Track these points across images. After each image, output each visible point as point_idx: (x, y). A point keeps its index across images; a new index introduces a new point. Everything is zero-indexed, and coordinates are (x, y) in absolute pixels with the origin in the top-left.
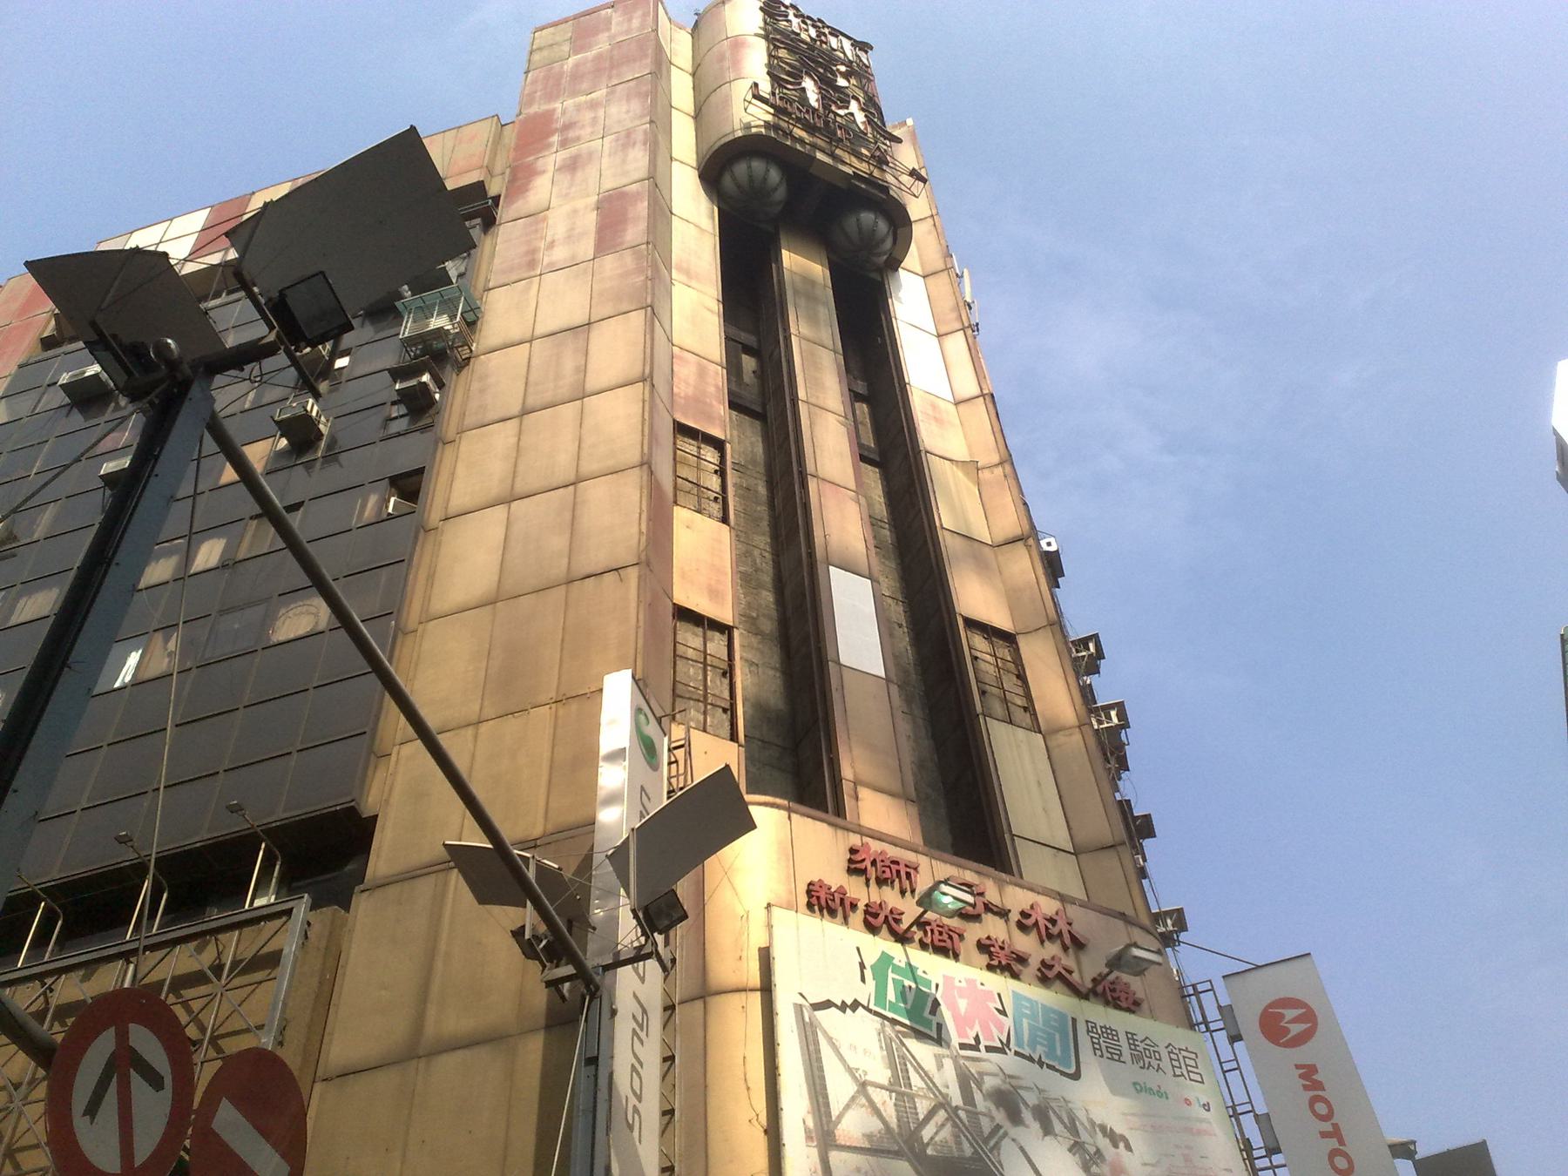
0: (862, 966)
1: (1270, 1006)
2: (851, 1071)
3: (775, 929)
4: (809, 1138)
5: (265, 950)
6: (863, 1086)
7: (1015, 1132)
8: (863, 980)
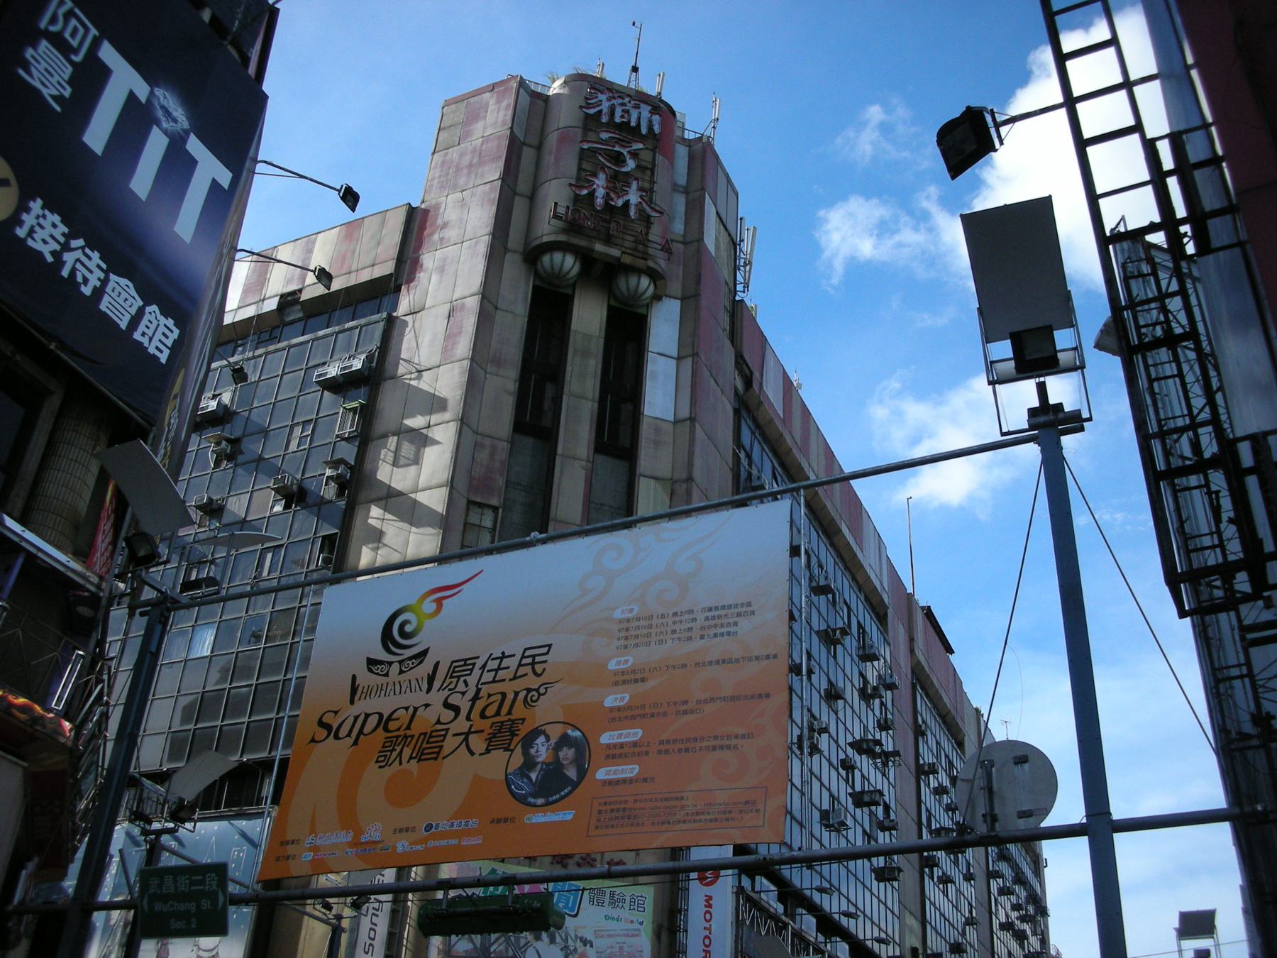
7: (538, 945)
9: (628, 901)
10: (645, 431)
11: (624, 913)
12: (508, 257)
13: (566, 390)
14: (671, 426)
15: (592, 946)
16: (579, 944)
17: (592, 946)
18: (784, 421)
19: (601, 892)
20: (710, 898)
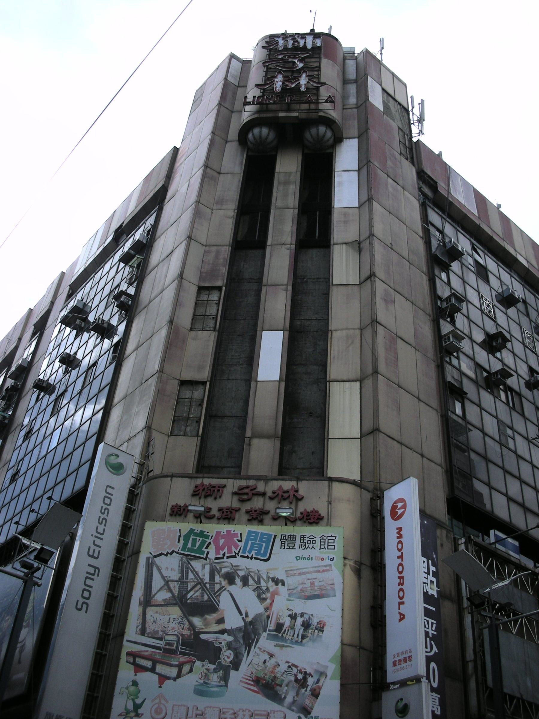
0: (180, 536)
1: (394, 503)
2: (163, 577)
3: (341, 615)
4: (140, 604)
5: (9, 537)
6: (167, 583)
7: (232, 588)
8: (179, 542)
9: (318, 540)
10: (336, 217)
11: (315, 553)
12: (228, 145)
13: (273, 207)
14: (357, 210)
15: (283, 584)
16: (271, 584)
17: (283, 584)
18: (479, 218)
19: (292, 538)
20: (400, 529)
